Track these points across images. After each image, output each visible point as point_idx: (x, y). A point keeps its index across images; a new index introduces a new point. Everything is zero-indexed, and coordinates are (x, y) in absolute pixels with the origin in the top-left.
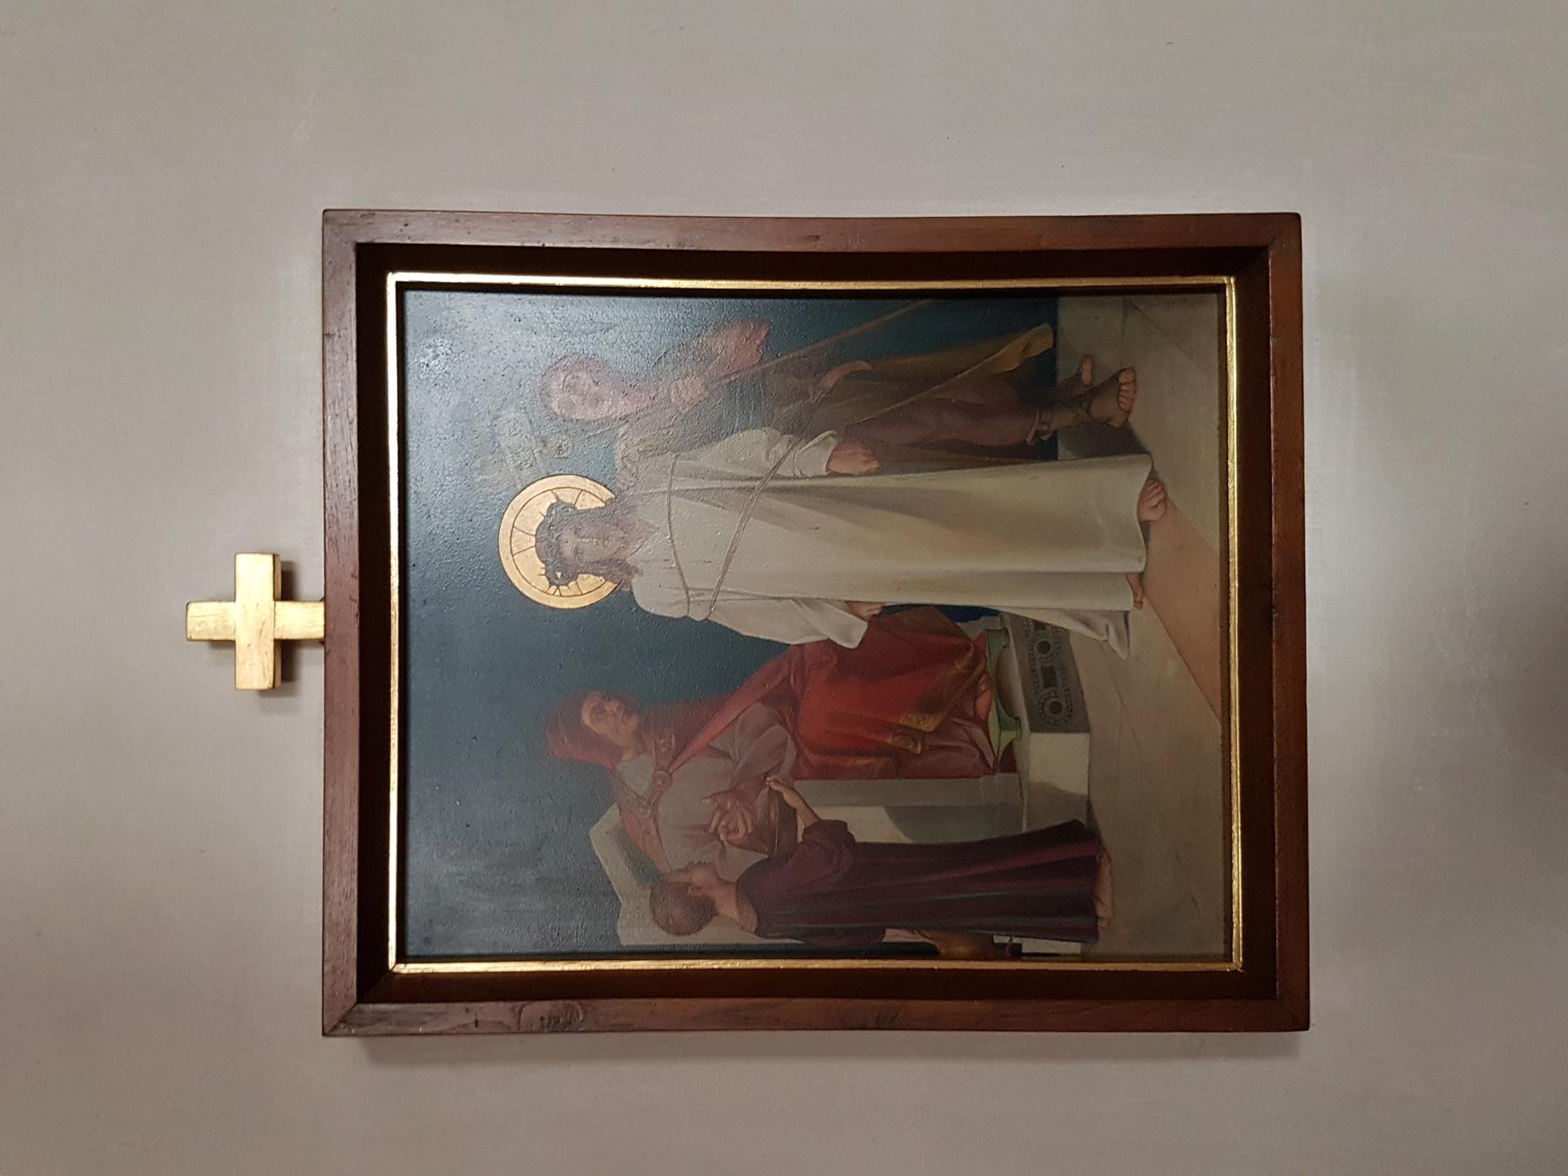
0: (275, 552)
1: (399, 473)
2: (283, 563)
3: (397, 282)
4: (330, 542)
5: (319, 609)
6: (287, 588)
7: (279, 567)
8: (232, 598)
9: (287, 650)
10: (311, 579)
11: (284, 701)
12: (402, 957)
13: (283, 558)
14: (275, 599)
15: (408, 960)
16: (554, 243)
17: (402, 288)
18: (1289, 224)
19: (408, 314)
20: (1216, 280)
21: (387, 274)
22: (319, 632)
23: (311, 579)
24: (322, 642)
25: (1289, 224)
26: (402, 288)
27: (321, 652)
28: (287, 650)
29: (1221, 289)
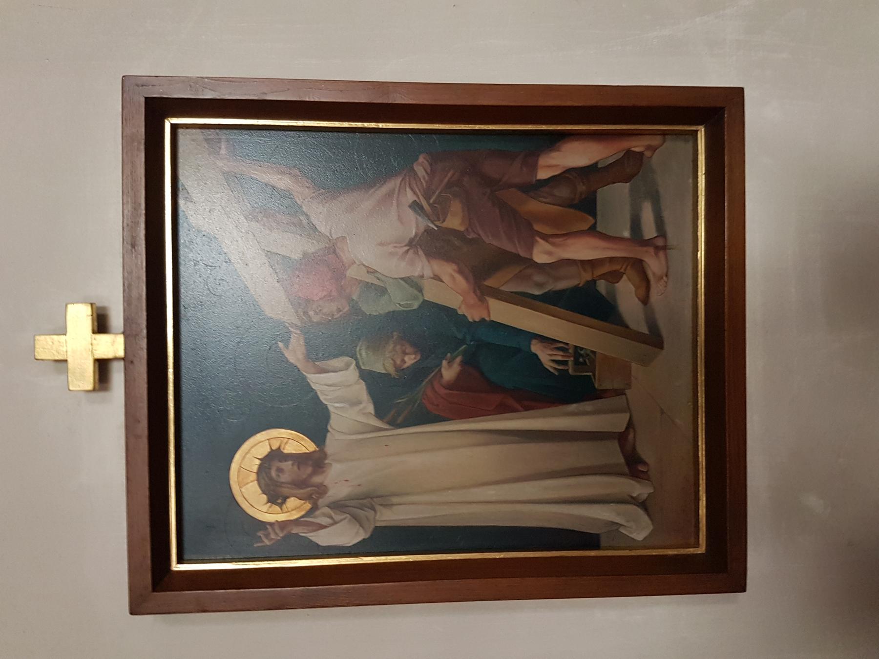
0: (92, 302)
1: (171, 187)
2: (98, 308)
3: (741, 91)
4: (128, 301)
5: (120, 339)
6: (101, 325)
7: (94, 310)
8: (65, 334)
9: (103, 366)
10: (117, 319)
11: (101, 395)
12: (180, 561)
13: (99, 304)
14: (94, 332)
15: (185, 562)
16: (300, 98)
17: (174, 127)
18: (738, 93)
19: (184, 448)
20: (694, 128)
21: (631, 234)
22: (121, 353)
23: (117, 319)
24: (123, 359)
25: (738, 93)
26: (174, 127)
27: (122, 363)
28: (103, 366)
29: (696, 132)
